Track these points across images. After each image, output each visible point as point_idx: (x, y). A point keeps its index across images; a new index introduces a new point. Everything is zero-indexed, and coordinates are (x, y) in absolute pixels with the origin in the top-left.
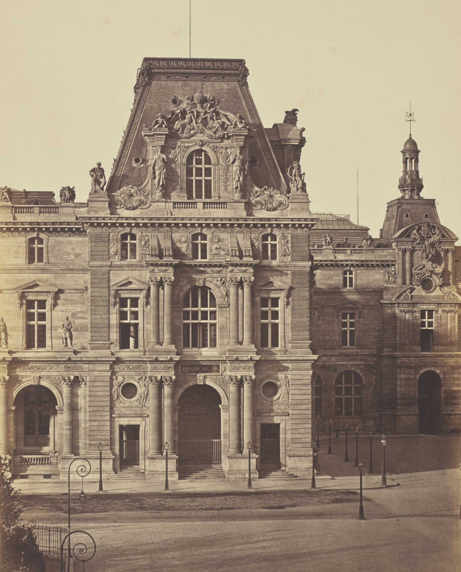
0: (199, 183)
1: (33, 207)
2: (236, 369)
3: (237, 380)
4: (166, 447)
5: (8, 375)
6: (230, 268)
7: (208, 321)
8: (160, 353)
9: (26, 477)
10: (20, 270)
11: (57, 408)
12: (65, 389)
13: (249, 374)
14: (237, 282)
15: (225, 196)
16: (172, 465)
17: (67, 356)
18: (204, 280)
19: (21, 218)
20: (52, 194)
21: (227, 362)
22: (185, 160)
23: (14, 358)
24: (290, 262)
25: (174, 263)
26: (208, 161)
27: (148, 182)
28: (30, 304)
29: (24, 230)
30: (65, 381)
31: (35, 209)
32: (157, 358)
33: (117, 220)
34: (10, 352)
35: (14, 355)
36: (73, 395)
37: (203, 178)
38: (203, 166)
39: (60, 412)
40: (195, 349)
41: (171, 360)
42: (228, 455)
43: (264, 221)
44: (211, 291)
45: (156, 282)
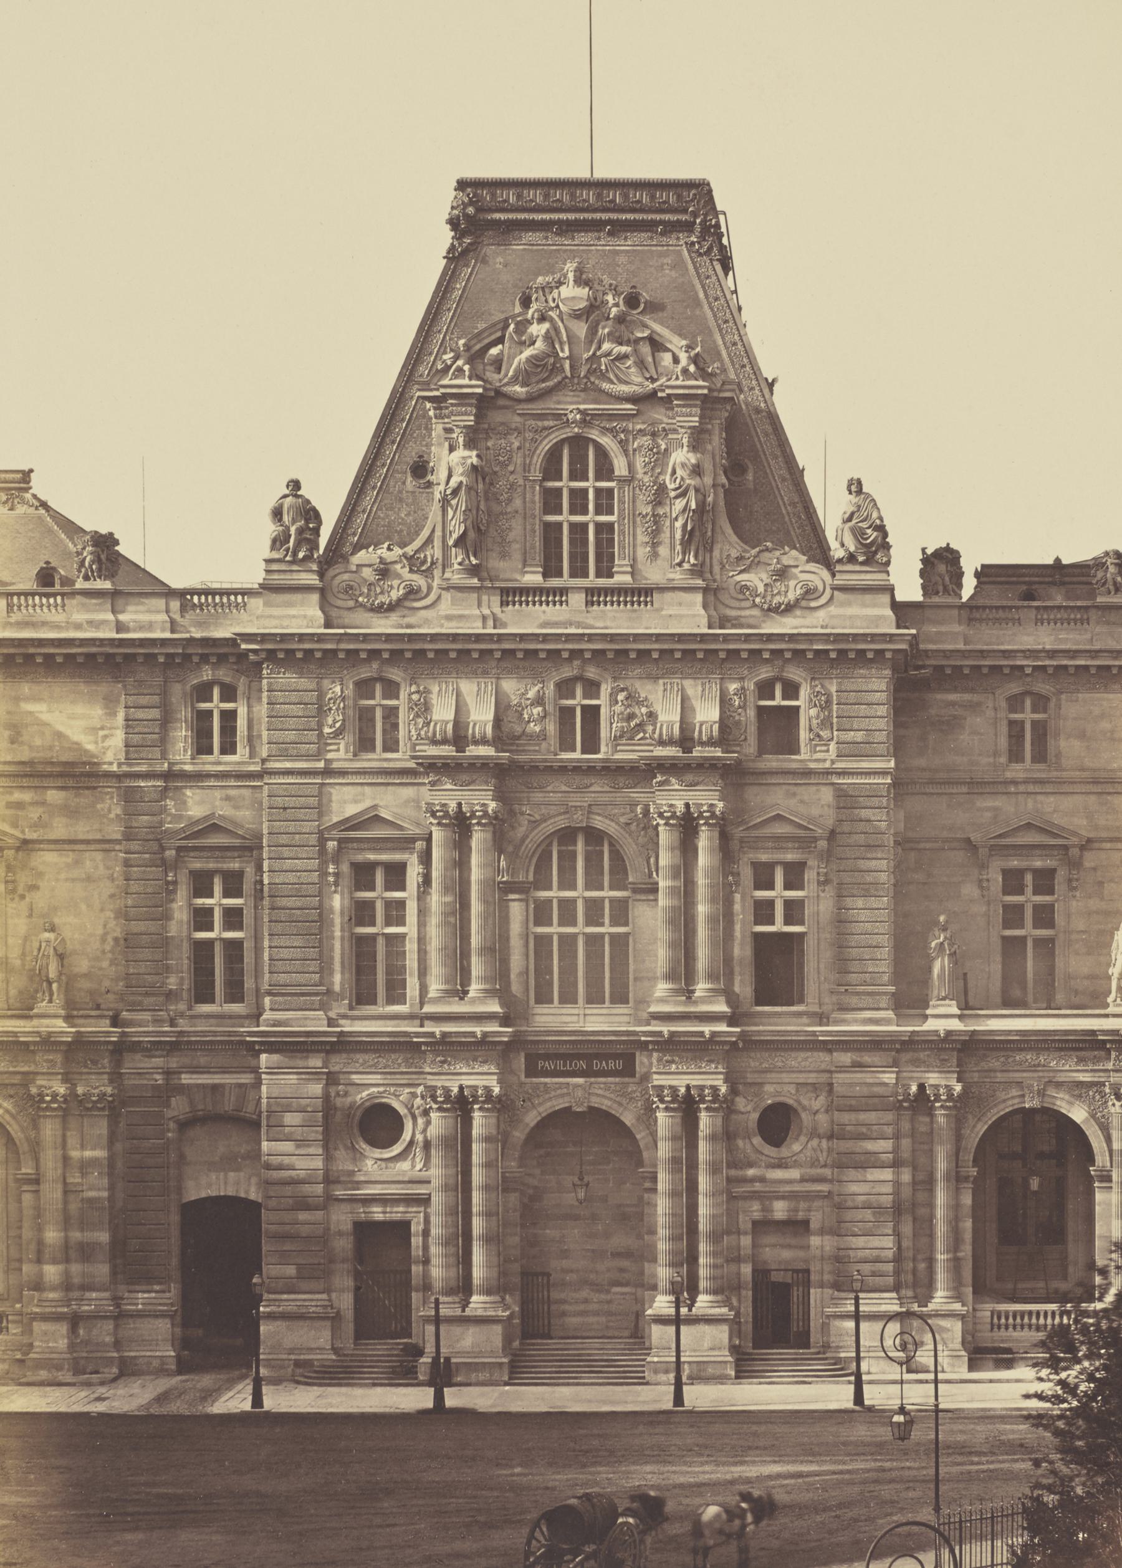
7: (554, 929)
15: (654, 574)
24: (833, 762)
26: (605, 470)
27: (433, 531)
37: (590, 517)
38: (590, 484)
40: (569, 1009)
43: (879, 642)
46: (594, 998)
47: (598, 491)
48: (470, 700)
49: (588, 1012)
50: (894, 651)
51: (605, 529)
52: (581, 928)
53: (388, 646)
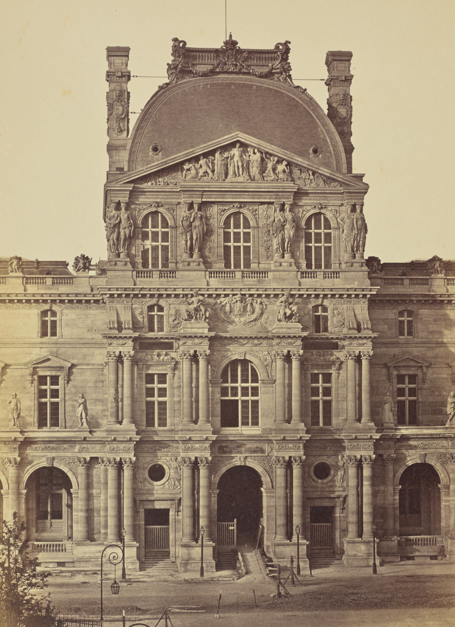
0: (318, 249)
1: (45, 278)
2: (186, 450)
3: (356, 459)
4: (202, 533)
5: (134, 456)
6: (278, 341)
8: (289, 432)
9: (412, 558)
10: (33, 345)
11: (72, 492)
13: (282, 456)
14: (355, 356)
16: (209, 552)
18: (245, 354)
19: (32, 289)
20: (65, 264)
21: (274, 442)
22: (222, 224)
23: (26, 438)
25: (133, 336)
28: (42, 380)
29: (37, 301)
30: (11, 463)
31: (47, 279)
32: (371, 436)
33: (140, 291)
35: (26, 435)
36: (89, 476)
39: (6, 496)
41: (371, 438)
42: (182, 543)
44: (252, 364)
47: (245, 233)
49: (243, 429)
51: (165, 248)
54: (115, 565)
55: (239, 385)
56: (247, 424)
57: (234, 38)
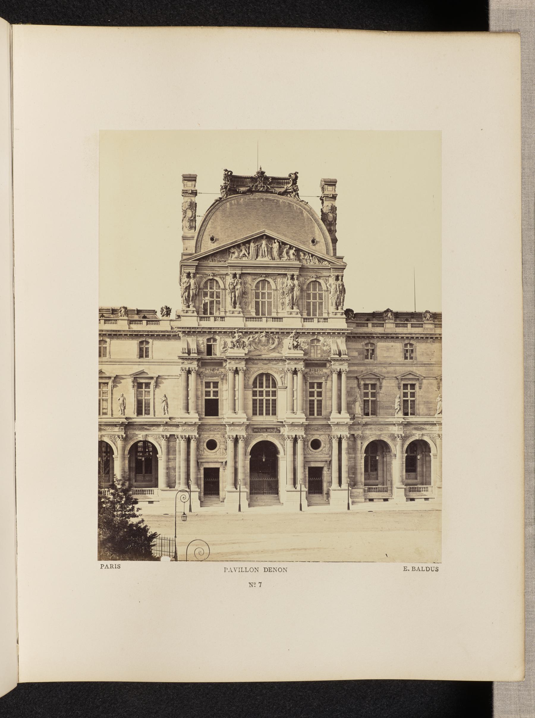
12: (163, 443)
17: (165, 421)
23: (129, 422)
31: (143, 321)
34: (126, 418)
40: (261, 417)
45: (243, 370)
46: (268, 414)
48: (190, 342)
49: (266, 417)
50: (347, 333)
52: (265, 397)
53: (381, 336)
54: (184, 502)
55: (264, 389)
56: (269, 414)
57: (263, 170)
